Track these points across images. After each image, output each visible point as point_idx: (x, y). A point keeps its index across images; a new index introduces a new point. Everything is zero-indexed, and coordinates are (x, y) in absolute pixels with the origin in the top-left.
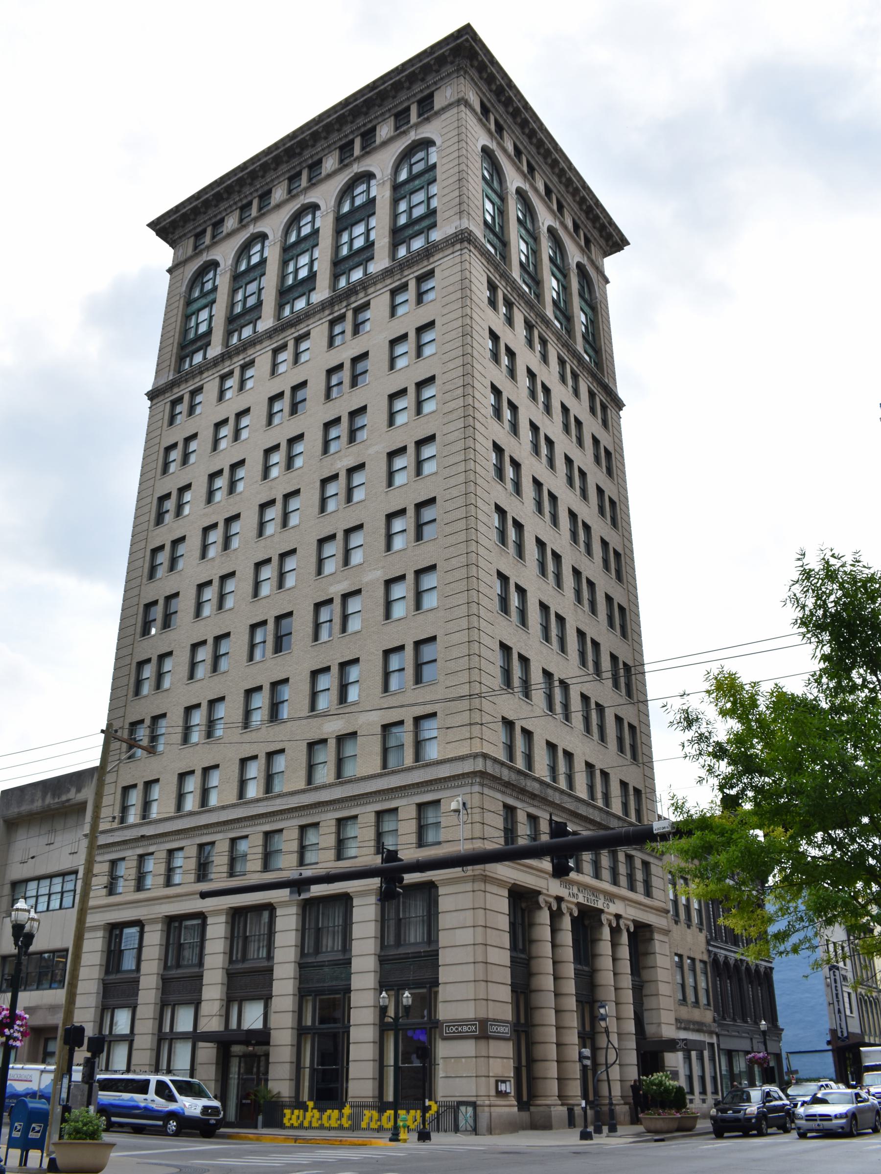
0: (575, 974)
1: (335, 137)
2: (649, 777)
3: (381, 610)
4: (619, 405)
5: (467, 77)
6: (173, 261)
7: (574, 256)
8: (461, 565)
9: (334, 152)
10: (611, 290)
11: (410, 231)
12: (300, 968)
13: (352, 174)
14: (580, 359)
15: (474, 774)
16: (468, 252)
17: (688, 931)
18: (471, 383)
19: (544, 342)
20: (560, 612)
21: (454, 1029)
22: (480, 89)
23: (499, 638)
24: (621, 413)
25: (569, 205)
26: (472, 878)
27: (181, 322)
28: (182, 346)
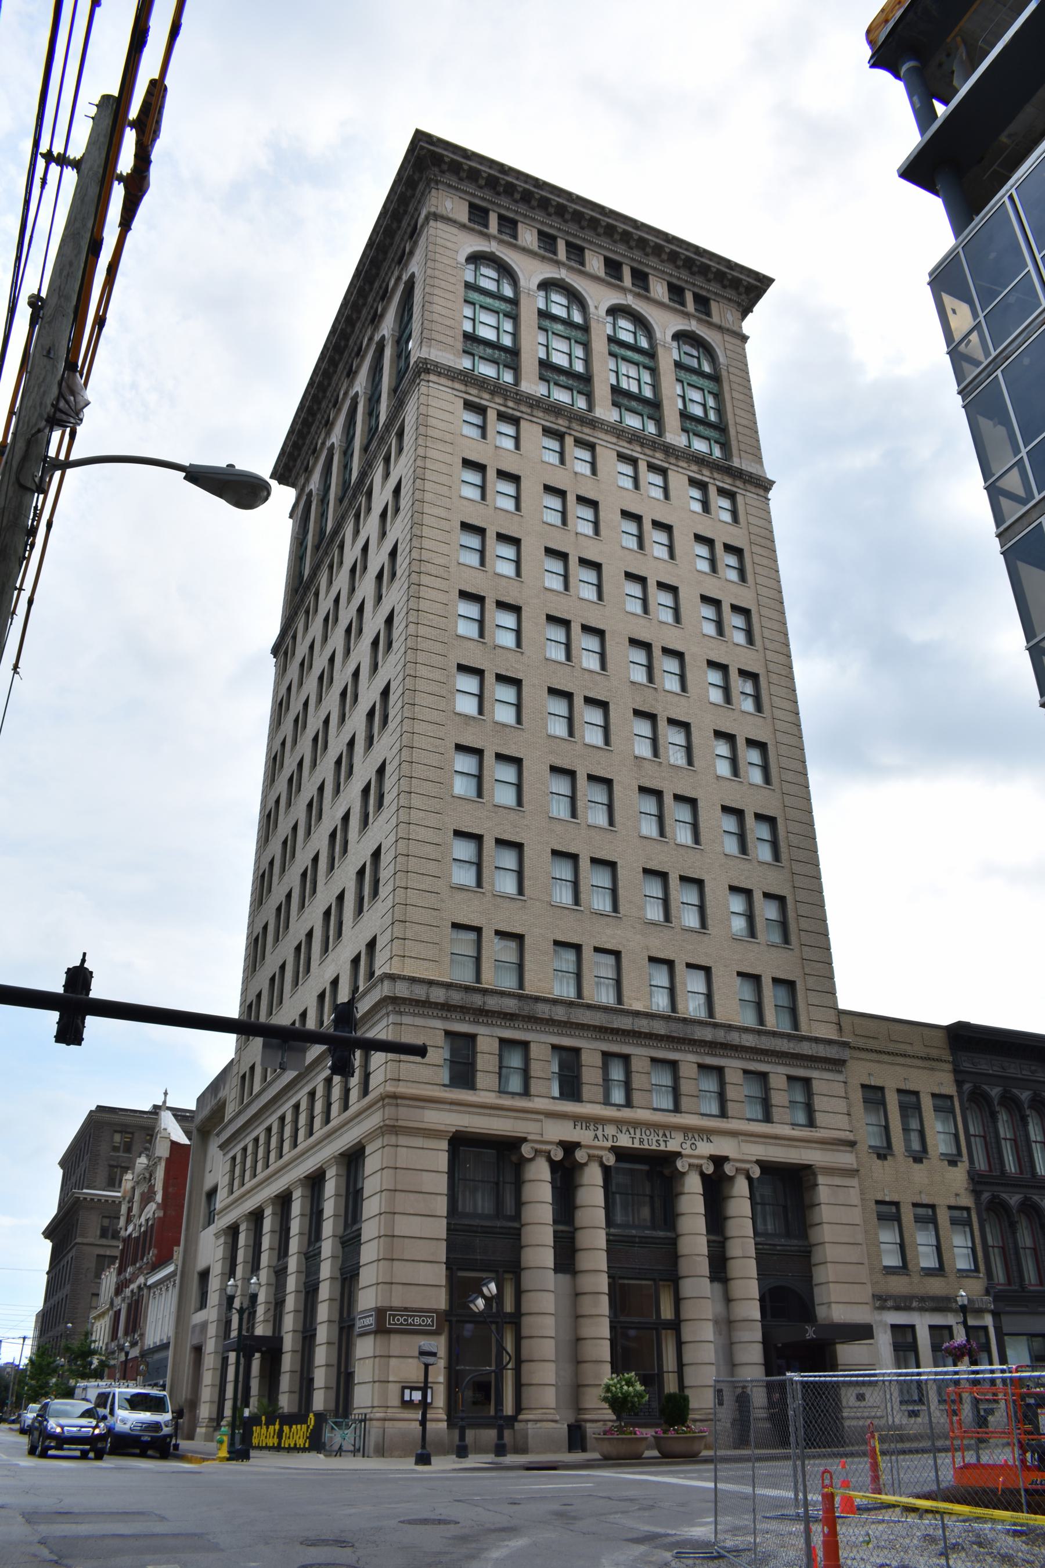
0: (608, 1241)
12: (307, 1259)
21: (402, 1320)
25: (655, 269)
26: (379, 1131)
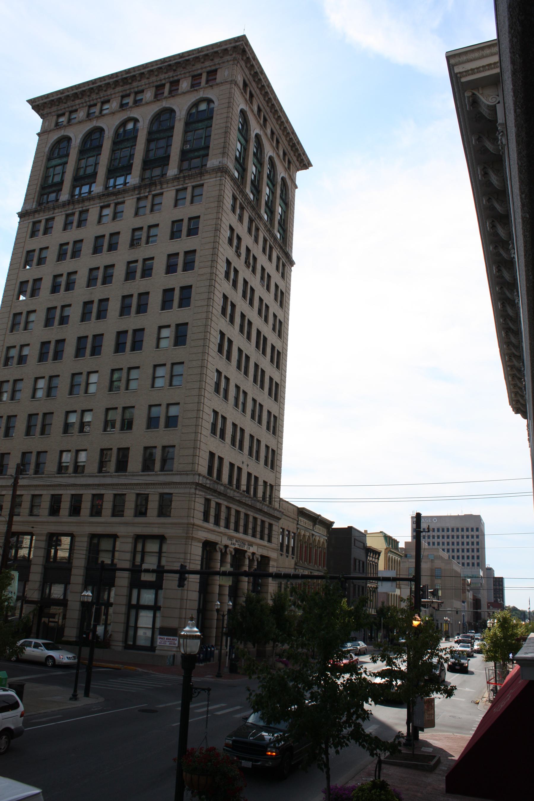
1: (154, 79)
2: (278, 478)
3: (150, 382)
4: (292, 263)
5: (238, 65)
6: (41, 128)
7: (281, 173)
8: (198, 366)
9: (152, 88)
10: (298, 193)
11: (192, 155)
13: (161, 107)
14: (275, 238)
15: (193, 483)
16: (224, 179)
17: (287, 559)
18: (216, 260)
19: (257, 229)
20: (245, 390)
22: (245, 73)
23: (213, 407)
24: (293, 268)
25: (283, 141)
27: (44, 171)
28: (43, 188)
